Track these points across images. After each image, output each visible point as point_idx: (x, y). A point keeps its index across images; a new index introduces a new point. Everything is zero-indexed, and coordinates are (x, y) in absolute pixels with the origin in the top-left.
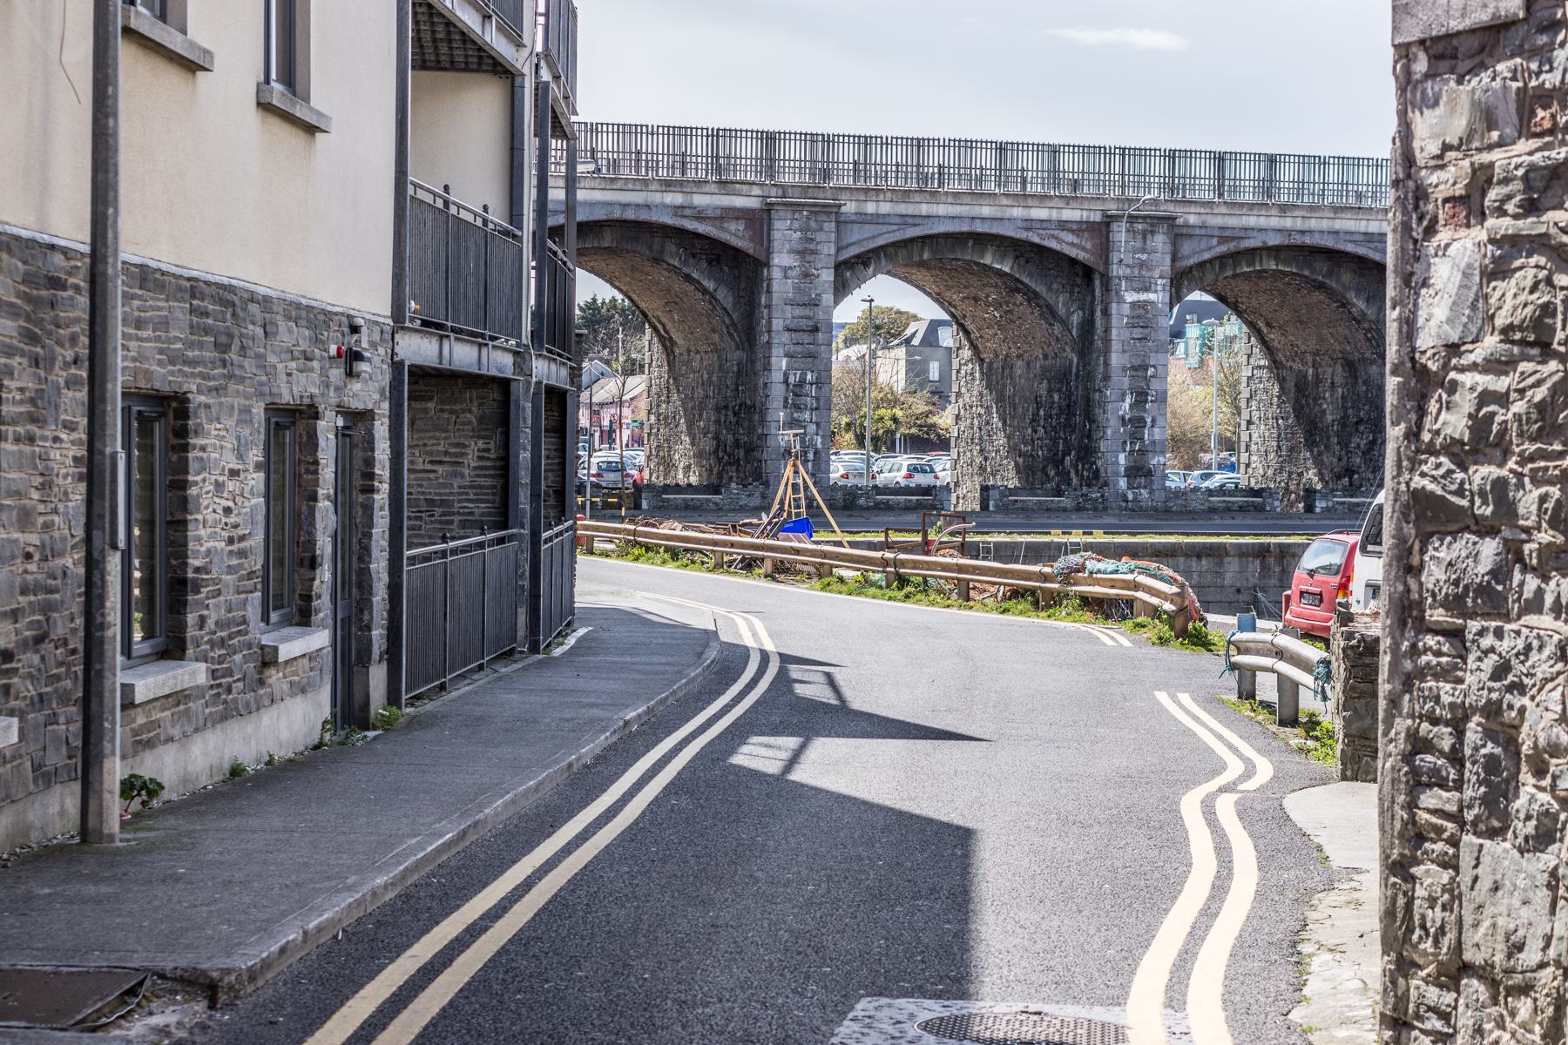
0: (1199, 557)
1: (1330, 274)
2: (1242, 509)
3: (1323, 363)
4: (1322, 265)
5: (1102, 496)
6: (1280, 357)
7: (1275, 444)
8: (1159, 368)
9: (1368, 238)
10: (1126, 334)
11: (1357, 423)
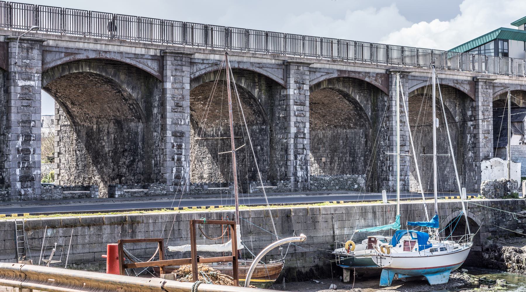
0: (89, 226)
1: (115, 75)
2: (80, 197)
3: (103, 122)
4: (111, 71)
5: (8, 193)
6: (78, 120)
7: (75, 164)
8: (37, 122)
9: (136, 56)
10: (19, 103)
11: (123, 151)
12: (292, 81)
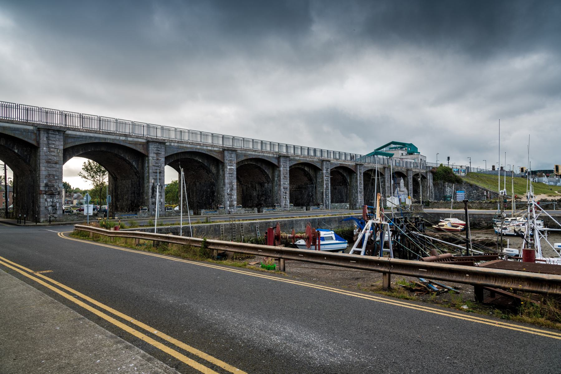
10: (228, 175)
12: (324, 167)
